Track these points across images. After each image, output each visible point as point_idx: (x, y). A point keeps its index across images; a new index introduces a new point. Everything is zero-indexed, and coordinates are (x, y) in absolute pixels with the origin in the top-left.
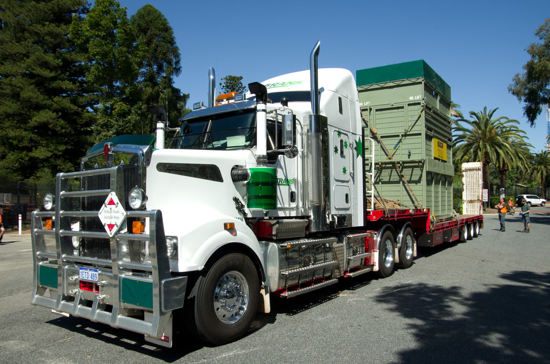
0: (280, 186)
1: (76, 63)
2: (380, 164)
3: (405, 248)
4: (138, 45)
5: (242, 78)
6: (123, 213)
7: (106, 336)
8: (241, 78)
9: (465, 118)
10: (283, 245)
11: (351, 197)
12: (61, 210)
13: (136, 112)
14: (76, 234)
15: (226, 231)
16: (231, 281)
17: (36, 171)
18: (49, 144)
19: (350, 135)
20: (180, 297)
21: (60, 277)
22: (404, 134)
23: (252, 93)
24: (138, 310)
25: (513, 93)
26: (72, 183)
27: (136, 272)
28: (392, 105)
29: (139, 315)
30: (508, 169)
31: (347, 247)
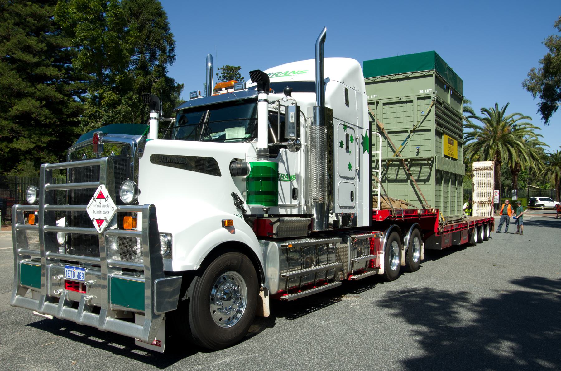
0: (282, 182)
1: (62, 48)
2: (387, 161)
3: (412, 250)
4: (129, 31)
5: (241, 68)
6: (113, 208)
7: (92, 340)
8: (240, 68)
9: (477, 115)
10: (284, 244)
11: (357, 195)
12: (46, 203)
13: (127, 103)
14: (61, 229)
15: (224, 228)
16: (228, 282)
17: (17, 164)
18: (32, 135)
19: (356, 129)
20: (174, 299)
21: (43, 277)
22: (412, 129)
23: (253, 82)
24: (128, 312)
25: (528, 89)
26: (56, 177)
27: (126, 271)
28: (401, 99)
29: (130, 318)
30: (520, 169)
31: (352, 248)
